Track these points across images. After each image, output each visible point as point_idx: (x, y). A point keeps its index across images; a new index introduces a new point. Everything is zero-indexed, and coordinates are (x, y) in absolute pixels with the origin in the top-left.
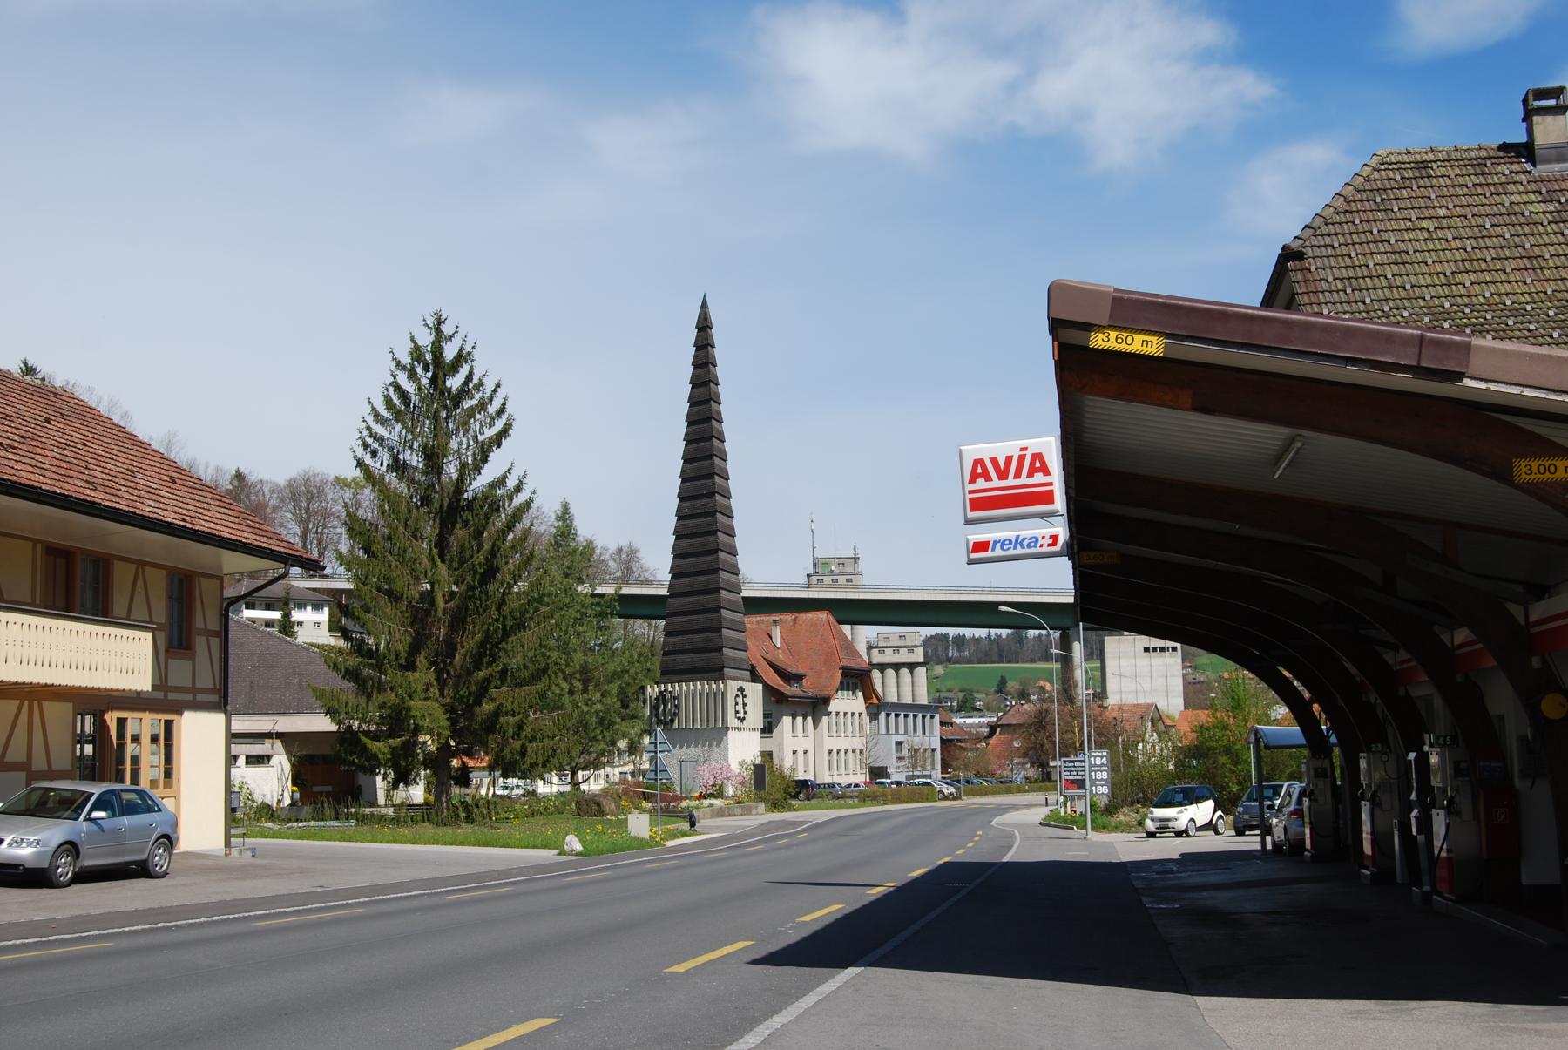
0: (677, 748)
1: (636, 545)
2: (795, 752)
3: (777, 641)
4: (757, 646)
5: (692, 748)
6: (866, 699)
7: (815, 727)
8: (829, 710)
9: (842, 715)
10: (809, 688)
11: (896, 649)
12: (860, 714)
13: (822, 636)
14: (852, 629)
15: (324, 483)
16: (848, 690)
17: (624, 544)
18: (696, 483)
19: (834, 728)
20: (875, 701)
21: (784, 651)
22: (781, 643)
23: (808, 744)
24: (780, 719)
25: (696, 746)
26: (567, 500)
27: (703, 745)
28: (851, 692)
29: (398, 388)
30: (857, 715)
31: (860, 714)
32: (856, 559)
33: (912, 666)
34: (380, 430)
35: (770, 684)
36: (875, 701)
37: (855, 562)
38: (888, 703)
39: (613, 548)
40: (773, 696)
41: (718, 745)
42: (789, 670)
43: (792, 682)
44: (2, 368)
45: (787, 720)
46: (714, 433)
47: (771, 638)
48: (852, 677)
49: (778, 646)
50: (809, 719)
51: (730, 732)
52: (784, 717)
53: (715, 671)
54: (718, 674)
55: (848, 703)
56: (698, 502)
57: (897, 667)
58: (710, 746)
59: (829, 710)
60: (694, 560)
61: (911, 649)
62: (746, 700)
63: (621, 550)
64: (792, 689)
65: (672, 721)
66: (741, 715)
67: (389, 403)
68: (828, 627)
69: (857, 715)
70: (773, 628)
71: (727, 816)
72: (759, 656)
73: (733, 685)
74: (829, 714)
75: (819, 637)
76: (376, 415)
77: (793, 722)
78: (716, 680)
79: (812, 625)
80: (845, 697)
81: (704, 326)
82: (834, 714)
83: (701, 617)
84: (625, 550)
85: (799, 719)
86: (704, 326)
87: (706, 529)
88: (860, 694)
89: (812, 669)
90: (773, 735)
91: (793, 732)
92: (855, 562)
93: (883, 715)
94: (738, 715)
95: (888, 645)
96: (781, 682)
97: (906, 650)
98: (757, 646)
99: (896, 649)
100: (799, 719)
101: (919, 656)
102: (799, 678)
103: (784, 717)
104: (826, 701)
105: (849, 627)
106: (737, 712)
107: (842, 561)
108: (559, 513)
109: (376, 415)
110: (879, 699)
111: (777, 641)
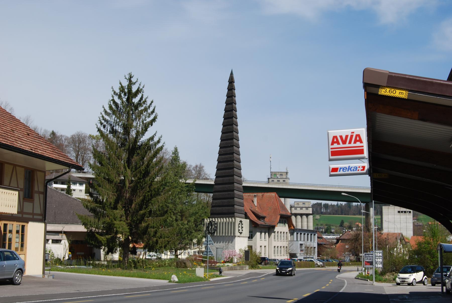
0: (216, 243)
1: (203, 165)
2: (261, 246)
3: (256, 203)
5: (221, 243)
7: (269, 237)
10: (267, 222)
11: (301, 208)
12: (287, 233)
13: (273, 202)
14: (285, 200)
15: (85, 137)
16: (282, 223)
18: (226, 141)
20: (292, 228)
21: (258, 208)
23: (266, 243)
24: (255, 233)
25: (223, 242)
27: (226, 242)
28: (283, 224)
29: (114, 102)
30: (285, 233)
31: (287, 233)
32: (287, 173)
33: (307, 215)
34: (107, 117)
36: (292, 228)
37: (287, 174)
38: (297, 229)
40: (254, 225)
41: (232, 243)
45: (258, 234)
49: (256, 205)
50: (267, 234)
51: (236, 238)
55: (282, 228)
57: (301, 215)
58: (228, 243)
61: (307, 208)
63: (197, 166)
64: (261, 222)
65: (214, 233)
66: (241, 231)
67: (111, 107)
69: (285, 233)
70: (254, 198)
74: (275, 232)
75: (272, 202)
76: (106, 112)
80: (281, 226)
81: (231, 81)
82: (276, 232)
84: (199, 166)
85: (263, 234)
86: (231, 81)
88: (287, 225)
92: (287, 174)
93: (295, 233)
95: (298, 206)
97: (305, 209)
99: (301, 208)
100: (263, 234)
101: (310, 211)
102: (264, 218)
104: (274, 227)
106: (239, 230)
109: (106, 112)
110: (294, 227)
111: (256, 203)
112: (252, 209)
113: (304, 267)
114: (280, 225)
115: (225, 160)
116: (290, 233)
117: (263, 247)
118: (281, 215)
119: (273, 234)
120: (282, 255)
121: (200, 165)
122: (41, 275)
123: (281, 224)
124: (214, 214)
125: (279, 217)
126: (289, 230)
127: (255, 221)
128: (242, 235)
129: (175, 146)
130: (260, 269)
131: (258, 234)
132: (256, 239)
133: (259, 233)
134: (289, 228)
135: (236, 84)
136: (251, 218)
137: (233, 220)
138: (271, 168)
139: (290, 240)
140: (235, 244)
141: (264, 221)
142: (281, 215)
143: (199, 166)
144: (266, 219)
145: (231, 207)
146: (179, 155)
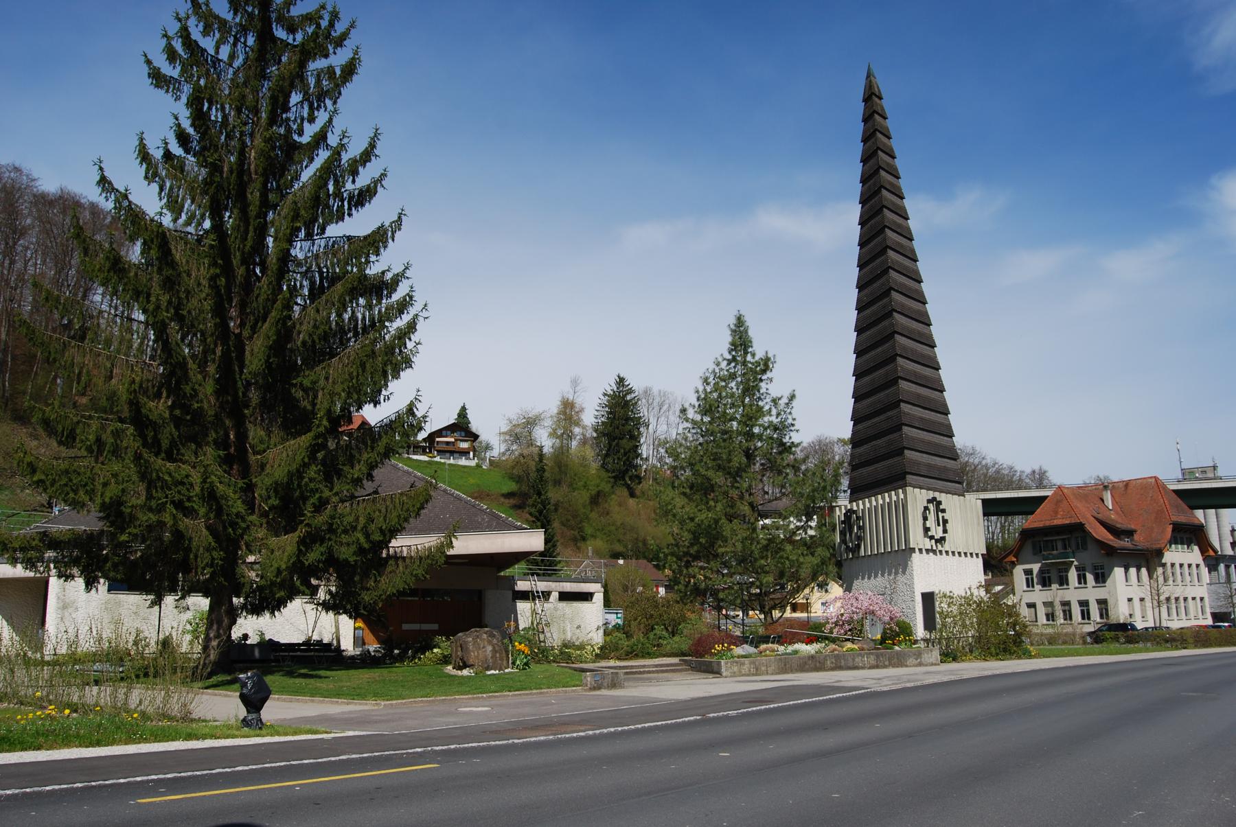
0: (866, 580)
1: (1045, 468)
2: (1130, 600)
3: (1109, 503)
4: (1088, 507)
5: (880, 578)
6: (1203, 552)
7: (1150, 577)
8: (1163, 561)
9: (1186, 566)
10: (1140, 540)
12: (1198, 566)
14: (1217, 514)
15: (832, 443)
16: (1182, 543)
17: (1036, 468)
18: (871, 266)
19: (1179, 577)
20: (1211, 553)
21: (1117, 513)
22: (1113, 505)
23: (1145, 592)
24: (1111, 570)
25: (883, 575)
26: (741, 313)
27: (890, 574)
28: (1186, 546)
30: (1194, 567)
31: (1198, 566)
32: (1215, 467)
35: (1097, 537)
36: (1211, 553)
37: (1215, 470)
38: (1226, 556)
39: (1028, 470)
40: (1103, 549)
41: (904, 572)
42: (1118, 526)
43: (1122, 537)
44: (3, 163)
45: (1118, 572)
46: (885, 203)
47: (1103, 501)
48: (1185, 532)
49: (1111, 508)
50: (1144, 571)
51: (916, 557)
52: (1116, 569)
53: (896, 480)
54: (900, 483)
55: (1181, 556)
56: (875, 285)
58: (896, 573)
59: (1163, 561)
60: (873, 353)
62: (946, 516)
63: (1034, 472)
64: (1122, 542)
65: (859, 546)
66: (937, 532)
68: (1156, 488)
69: (1194, 567)
70: (1104, 493)
71: (833, 669)
72: (1089, 516)
73: (917, 498)
74: (1164, 565)
75: (1149, 499)
77: (1126, 573)
78: (895, 489)
79: (1141, 489)
80: (1180, 550)
81: (871, 96)
82: (1169, 565)
83: (882, 417)
84: (1037, 471)
85: (1133, 571)
86: (871, 96)
87: (883, 313)
88: (1196, 548)
89: (1143, 526)
90: (1106, 584)
91: (1127, 581)
92: (1215, 470)
93: (1222, 567)
94: (930, 534)
96: (1111, 537)
98: (1088, 507)
100: (1133, 571)
102: (1130, 533)
103: (1116, 569)
104: (1159, 553)
105: (1202, 511)
106: (926, 530)
107: (1203, 469)
108: (733, 327)
110: (1215, 551)
111: (1109, 503)
112: (1099, 516)
113: (1220, 645)
114: (1176, 548)
115: (873, 319)
116: (1208, 565)
117: (1136, 602)
118: (1173, 524)
119: (1160, 570)
120: (1193, 618)
121: (1041, 469)
122: (283, 691)
123: (1180, 546)
124: (858, 491)
125: (1170, 528)
126: (1204, 560)
127: (1106, 541)
128: (947, 547)
129: (736, 313)
130: (1030, 657)
131: (1118, 572)
132: (1114, 582)
133: (1122, 569)
134: (1202, 555)
135: (887, 104)
136: (1095, 535)
137: (902, 496)
138: (1181, 462)
139: (1208, 582)
140: (911, 575)
141: (1132, 540)
142: (1173, 524)
143: (1037, 471)
144: (1136, 537)
145: (896, 459)
146: (750, 333)
